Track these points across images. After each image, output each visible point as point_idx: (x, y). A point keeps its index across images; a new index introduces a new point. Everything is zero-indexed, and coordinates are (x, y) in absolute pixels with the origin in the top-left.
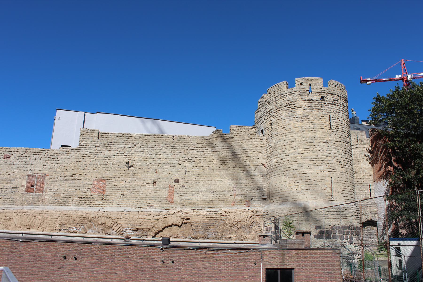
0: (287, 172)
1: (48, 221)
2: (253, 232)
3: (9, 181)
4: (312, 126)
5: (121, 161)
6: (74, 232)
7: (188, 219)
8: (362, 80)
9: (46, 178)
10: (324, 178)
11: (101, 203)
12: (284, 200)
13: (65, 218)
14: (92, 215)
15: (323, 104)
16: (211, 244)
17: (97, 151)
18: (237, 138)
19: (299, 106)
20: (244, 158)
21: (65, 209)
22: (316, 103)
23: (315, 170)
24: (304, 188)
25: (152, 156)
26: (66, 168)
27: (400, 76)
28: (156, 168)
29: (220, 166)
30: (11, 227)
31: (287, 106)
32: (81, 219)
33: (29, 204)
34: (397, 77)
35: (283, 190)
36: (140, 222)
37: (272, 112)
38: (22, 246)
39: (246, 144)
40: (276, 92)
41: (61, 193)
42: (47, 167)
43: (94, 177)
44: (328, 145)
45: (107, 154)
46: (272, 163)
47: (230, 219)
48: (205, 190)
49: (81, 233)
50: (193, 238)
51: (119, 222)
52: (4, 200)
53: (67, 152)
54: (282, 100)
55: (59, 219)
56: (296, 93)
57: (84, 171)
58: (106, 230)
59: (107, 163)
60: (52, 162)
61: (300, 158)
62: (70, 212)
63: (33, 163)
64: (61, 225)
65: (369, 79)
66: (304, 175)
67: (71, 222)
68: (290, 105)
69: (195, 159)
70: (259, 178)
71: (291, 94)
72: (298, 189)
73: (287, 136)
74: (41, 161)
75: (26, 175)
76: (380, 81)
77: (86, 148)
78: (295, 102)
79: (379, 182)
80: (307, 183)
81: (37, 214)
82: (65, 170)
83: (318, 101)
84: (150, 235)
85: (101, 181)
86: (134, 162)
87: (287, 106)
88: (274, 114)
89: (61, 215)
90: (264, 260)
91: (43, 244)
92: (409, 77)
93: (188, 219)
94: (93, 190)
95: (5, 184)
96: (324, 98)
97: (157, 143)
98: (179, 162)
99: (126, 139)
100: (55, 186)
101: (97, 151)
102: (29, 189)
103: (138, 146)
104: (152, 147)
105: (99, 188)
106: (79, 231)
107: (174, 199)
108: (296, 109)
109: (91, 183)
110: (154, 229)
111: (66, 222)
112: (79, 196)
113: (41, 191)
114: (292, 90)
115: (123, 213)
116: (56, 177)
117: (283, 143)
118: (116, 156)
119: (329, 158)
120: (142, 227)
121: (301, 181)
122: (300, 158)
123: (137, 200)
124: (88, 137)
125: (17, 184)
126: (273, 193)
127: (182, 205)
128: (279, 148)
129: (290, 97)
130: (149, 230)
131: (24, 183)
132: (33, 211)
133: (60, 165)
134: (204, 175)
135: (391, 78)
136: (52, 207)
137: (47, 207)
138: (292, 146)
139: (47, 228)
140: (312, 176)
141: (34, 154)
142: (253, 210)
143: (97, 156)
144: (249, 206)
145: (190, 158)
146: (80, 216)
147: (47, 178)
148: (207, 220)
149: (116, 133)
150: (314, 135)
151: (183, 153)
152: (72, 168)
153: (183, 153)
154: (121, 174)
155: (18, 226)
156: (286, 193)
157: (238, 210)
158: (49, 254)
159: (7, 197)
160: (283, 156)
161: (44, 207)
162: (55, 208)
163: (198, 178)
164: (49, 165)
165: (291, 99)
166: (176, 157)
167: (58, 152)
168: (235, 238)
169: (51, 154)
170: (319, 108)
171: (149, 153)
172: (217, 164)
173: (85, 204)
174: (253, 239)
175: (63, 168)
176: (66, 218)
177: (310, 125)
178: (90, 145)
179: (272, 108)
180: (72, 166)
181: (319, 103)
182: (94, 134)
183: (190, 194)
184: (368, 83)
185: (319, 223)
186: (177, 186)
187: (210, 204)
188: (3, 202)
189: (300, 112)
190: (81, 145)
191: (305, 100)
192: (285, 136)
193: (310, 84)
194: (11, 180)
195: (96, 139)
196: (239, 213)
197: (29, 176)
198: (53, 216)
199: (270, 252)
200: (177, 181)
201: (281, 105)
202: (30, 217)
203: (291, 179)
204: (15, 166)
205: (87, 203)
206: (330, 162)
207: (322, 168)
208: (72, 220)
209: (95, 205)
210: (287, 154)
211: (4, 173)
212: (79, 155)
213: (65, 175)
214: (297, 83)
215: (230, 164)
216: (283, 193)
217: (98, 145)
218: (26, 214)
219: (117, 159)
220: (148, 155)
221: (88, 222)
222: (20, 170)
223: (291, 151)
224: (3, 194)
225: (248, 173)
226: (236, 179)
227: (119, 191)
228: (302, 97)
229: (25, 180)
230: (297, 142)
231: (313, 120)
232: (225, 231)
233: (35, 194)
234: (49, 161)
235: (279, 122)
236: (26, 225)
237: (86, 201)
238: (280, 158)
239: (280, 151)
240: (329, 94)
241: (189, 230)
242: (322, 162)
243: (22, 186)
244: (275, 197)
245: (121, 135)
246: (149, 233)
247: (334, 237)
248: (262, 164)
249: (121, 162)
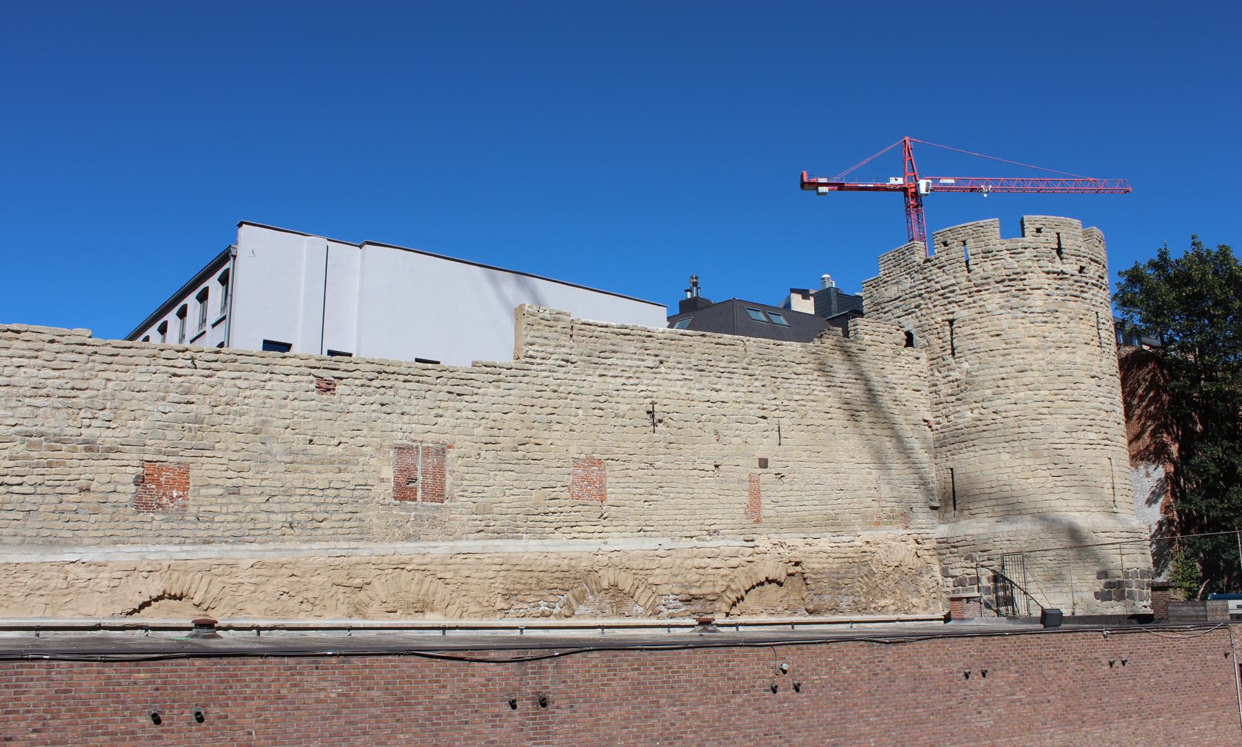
0: (1014, 444)
1: (472, 587)
2: (924, 591)
3: (343, 465)
4: (1066, 337)
5: (636, 406)
6: (543, 615)
7: (797, 564)
8: (805, 180)
9: (448, 456)
11: (599, 528)
12: (1010, 508)
13: (516, 574)
14: (584, 564)
16: (324, 634)
17: (570, 376)
18: (871, 351)
20: (890, 404)
21: (510, 547)
22: (1071, 282)
25: (702, 392)
26: (497, 424)
27: (900, 181)
28: (717, 426)
29: (847, 423)
30: (370, 611)
31: (1003, 281)
32: (556, 575)
33: (408, 538)
34: (893, 181)
35: (1007, 488)
36: (697, 577)
37: (953, 292)
38: (890, 655)
39: (889, 368)
40: (970, 243)
41: (493, 500)
42: (447, 422)
43: (573, 452)
45: (599, 384)
46: (960, 421)
47: (879, 561)
48: (822, 488)
49: (559, 616)
50: (811, 612)
51: (651, 580)
52: (333, 524)
53: (495, 377)
54: (988, 266)
55: (501, 580)
56: (1028, 253)
57: (546, 434)
58: (619, 605)
59: (601, 413)
60: (459, 405)
61: (1046, 411)
62: (526, 556)
63: (406, 409)
64: (507, 596)
65: (824, 180)
67: (533, 586)
68: (1012, 281)
69: (793, 404)
70: (922, 456)
71: (1014, 253)
74: (428, 403)
75: (391, 447)
76: (851, 189)
77: (543, 367)
81: (438, 568)
82: (496, 432)
84: (720, 611)
85: (594, 464)
86: (665, 408)
87: (1003, 281)
88: (962, 298)
89: (504, 567)
91: (925, 644)
92: (923, 185)
93: (797, 564)
94: (576, 489)
95: (331, 476)
97: (710, 357)
98: (762, 413)
99: (640, 345)
100: (475, 479)
101: (570, 376)
102: (404, 491)
103: (669, 364)
104: (700, 367)
105: (590, 484)
106: (555, 611)
107: (764, 513)
108: (1029, 291)
109: (568, 470)
110: (728, 593)
111: (519, 587)
112: (541, 510)
113: (438, 494)
114: (1019, 243)
115: (657, 553)
116: (474, 453)
117: (997, 373)
118: (622, 393)
119: (1103, 414)
120: (704, 590)
121: (1051, 466)
122: (1046, 411)
123: (682, 517)
124: (547, 334)
125: (366, 474)
126: (971, 492)
127: (780, 527)
128: (987, 384)
130: (718, 597)
131: (388, 472)
132: (427, 559)
133: (481, 414)
134: (818, 448)
135: (879, 184)
136: (473, 544)
137: (462, 545)
138: (1025, 380)
139: (473, 608)
140: (1078, 455)
141: (405, 381)
143: (574, 389)
145: (786, 403)
146: (555, 569)
147: (451, 454)
148: (835, 566)
149: (614, 324)
151: (769, 389)
152: (515, 425)
153: (769, 389)
154: (639, 445)
155: (390, 607)
156: (1014, 494)
157: (890, 536)
158: (939, 670)
159: (343, 516)
160: (999, 403)
161: (451, 544)
162: (483, 547)
163: (804, 456)
164: (452, 416)
165: (1016, 265)
166: (755, 397)
167: (473, 376)
168: (894, 608)
169: (454, 381)
170: (1077, 293)
171: (698, 386)
172: (840, 418)
173: (557, 534)
174: (925, 609)
175: (491, 424)
176: (519, 574)
177: (1061, 333)
178: (554, 357)
179: (953, 281)
180: (515, 420)
182: (561, 324)
183: (794, 498)
184: (821, 189)
185: (1103, 564)
186: (766, 476)
187: (834, 523)
188: (331, 531)
189: (1037, 301)
190: (531, 357)
191: (1048, 273)
194: (348, 462)
195: (564, 339)
196: (895, 544)
197: (400, 449)
198: (481, 571)
200: (764, 463)
202: (418, 576)
203: (1028, 462)
204: (353, 416)
205: (564, 529)
207: (1093, 436)
208: (534, 581)
209: (583, 535)
211: (325, 440)
212: (530, 386)
213: (497, 447)
214: (1030, 229)
215: (866, 418)
216: (1005, 494)
217: (572, 358)
218: (409, 567)
219: (626, 401)
220: (694, 392)
221: (574, 583)
222: (371, 429)
223: (1022, 395)
224: (332, 508)
225: (899, 439)
226: (880, 459)
227: (638, 491)
228: (1042, 263)
229: (388, 460)
230: (1036, 374)
232: (873, 592)
233: (421, 505)
234: (451, 404)
236: (412, 600)
237: (561, 524)
238: (991, 410)
239: (988, 392)
241: (800, 591)
242: (1092, 423)
243: (382, 480)
244: (982, 504)
245: (628, 331)
246: (718, 605)
247: (1131, 596)
249: (634, 410)
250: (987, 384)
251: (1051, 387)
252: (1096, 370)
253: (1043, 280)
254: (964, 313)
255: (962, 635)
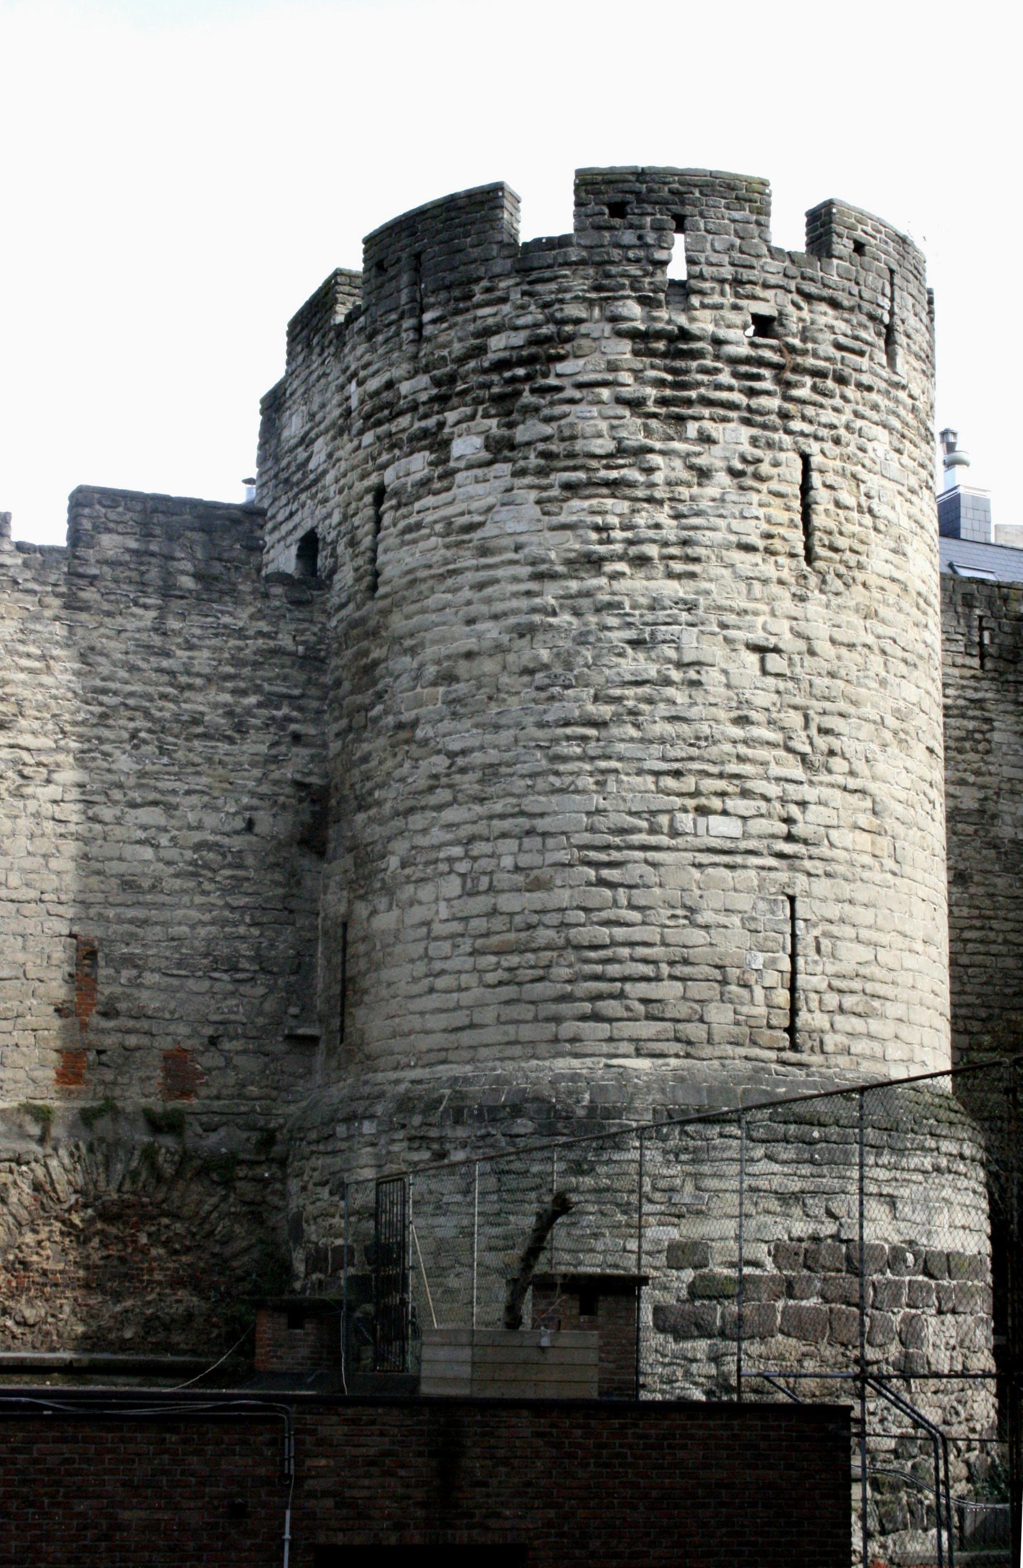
73: (489, 591)
90: (310, 1484)
108: (570, 393)
138: (526, 659)
192: (481, 586)
199: (354, 1421)
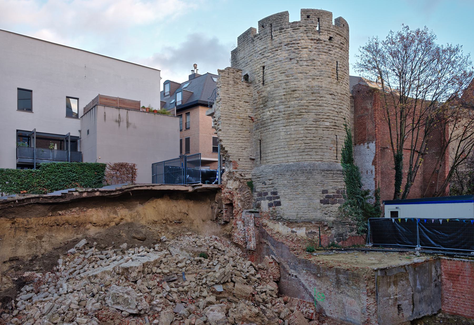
0: (287, 127)
10: (330, 137)
15: (331, 46)
19: (305, 47)
23: (321, 126)
24: (308, 147)
31: (288, 44)
44: (334, 97)
61: (304, 111)
66: (309, 131)
72: (301, 148)
73: (287, 84)
78: (300, 40)
79: (362, 144)
80: (312, 141)
83: (326, 43)
87: (288, 44)
96: (333, 39)
108: (300, 49)
129: (292, 33)
138: (295, 96)
142: (240, 172)
144: (236, 168)
150: (320, 84)
181: (326, 45)
191: (312, 39)
193: (319, 19)
201: (280, 43)
206: (336, 118)
207: (328, 124)
210: (288, 106)
223: (293, 103)
228: (309, 34)
230: (300, 92)
231: (320, 66)
235: (276, 66)
238: (278, 111)
240: (337, 34)
248: (249, 117)
250: (276, 98)
251: (307, 98)
252: (333, 91)
253: (309, 44)
254: (269, 62)
255: (417, 138)
